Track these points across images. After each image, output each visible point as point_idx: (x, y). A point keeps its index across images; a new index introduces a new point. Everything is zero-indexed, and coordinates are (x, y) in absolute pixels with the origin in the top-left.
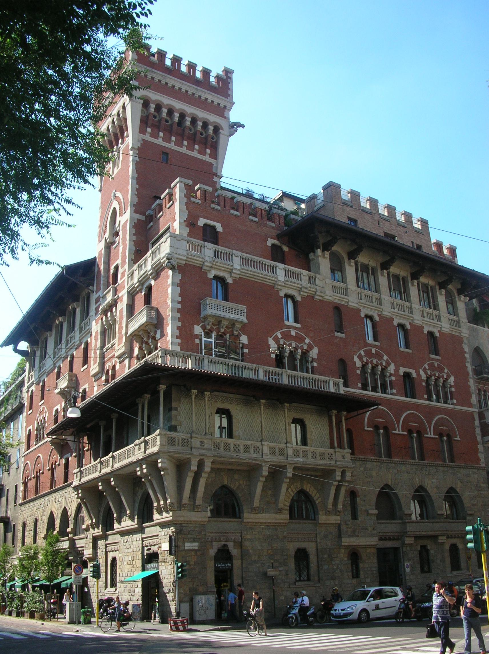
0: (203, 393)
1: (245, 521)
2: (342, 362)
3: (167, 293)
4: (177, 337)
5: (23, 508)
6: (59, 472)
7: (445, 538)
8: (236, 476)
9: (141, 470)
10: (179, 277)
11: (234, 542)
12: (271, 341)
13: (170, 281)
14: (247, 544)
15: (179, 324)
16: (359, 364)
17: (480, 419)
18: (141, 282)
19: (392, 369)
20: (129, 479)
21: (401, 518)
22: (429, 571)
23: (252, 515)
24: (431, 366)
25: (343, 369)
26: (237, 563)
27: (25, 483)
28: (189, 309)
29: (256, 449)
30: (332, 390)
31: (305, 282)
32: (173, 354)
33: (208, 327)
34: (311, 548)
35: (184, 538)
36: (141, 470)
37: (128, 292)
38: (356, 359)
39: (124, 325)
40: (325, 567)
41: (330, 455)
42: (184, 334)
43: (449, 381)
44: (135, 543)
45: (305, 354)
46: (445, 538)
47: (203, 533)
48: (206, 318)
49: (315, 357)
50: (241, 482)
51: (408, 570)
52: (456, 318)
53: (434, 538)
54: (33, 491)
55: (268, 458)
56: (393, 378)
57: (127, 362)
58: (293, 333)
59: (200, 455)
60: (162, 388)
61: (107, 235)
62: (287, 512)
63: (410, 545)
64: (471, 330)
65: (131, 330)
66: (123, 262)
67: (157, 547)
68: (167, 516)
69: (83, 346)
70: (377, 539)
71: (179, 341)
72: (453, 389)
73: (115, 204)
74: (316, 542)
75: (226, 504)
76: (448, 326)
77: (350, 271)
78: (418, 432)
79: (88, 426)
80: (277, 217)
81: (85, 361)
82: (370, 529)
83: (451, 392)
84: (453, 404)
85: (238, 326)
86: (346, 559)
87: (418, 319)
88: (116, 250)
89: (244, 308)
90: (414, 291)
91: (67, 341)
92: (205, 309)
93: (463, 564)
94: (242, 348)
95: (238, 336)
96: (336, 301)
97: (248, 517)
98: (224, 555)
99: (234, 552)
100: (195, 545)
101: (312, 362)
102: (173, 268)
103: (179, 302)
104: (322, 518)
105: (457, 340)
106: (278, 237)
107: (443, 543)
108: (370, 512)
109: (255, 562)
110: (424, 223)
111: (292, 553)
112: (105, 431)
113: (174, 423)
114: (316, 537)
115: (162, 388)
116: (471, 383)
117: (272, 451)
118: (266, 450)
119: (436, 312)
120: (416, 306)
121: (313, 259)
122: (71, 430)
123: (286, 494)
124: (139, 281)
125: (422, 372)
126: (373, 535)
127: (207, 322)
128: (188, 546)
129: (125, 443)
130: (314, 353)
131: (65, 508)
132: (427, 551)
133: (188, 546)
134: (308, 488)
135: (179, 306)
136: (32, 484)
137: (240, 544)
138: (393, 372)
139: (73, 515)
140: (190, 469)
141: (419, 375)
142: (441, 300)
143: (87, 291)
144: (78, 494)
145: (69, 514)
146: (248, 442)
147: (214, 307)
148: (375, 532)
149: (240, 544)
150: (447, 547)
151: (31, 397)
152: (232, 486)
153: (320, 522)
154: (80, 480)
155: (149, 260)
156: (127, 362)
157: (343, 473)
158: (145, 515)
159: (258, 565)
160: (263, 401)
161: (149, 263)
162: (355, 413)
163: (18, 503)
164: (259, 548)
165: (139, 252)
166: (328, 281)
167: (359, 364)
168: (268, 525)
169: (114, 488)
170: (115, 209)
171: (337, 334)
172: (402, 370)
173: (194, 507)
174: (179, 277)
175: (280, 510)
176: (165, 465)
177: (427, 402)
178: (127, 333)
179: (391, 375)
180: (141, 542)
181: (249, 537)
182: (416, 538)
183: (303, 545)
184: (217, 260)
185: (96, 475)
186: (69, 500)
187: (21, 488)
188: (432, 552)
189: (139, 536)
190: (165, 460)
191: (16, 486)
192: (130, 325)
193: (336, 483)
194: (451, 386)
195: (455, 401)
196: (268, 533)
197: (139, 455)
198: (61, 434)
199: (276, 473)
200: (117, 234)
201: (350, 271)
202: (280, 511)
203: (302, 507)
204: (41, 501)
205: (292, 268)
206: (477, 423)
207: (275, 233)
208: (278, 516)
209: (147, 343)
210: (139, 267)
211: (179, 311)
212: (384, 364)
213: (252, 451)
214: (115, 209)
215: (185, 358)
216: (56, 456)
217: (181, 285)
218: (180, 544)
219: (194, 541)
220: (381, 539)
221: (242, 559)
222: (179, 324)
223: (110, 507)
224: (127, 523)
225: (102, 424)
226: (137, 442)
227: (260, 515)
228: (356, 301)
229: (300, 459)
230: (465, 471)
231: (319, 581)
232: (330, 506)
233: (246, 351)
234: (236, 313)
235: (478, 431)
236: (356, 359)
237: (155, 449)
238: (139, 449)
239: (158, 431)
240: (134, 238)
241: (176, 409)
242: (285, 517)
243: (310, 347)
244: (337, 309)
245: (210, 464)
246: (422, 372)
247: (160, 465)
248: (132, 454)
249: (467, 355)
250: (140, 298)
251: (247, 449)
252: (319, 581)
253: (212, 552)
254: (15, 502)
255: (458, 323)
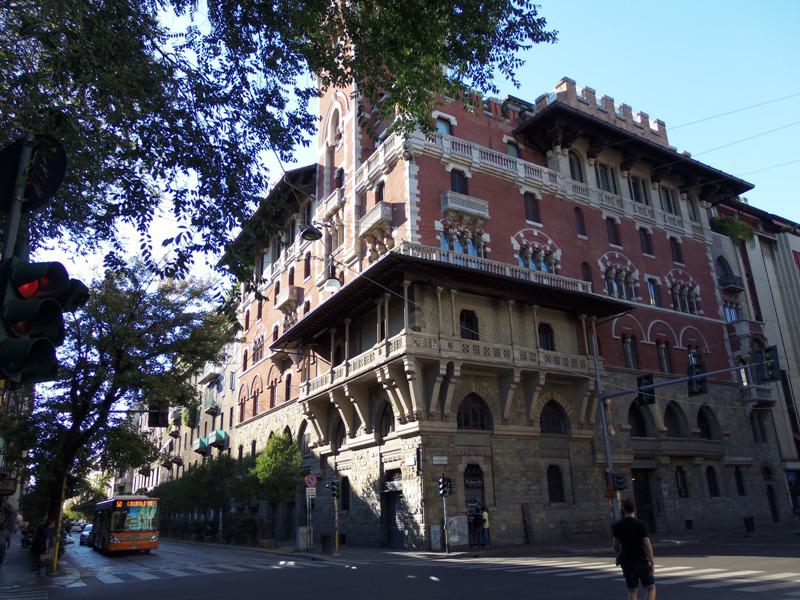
0: (449, 291)
1: (495, 433)
2: (585, 265)
3: (402, 186)
4: (418, 232)
5: (239, 430)
6: (281, 389)
7: (701, 459)
8: (485, 384)
9: (383, 375)
10: (416, 168)
11: (485, 456)
12: (513, 241)
13: (407, 173)
14: (497, 458)
15: (419, 219)
16: (603, 268)
17: (729, 332)
18: (372, 180)
19: (636, 274)
20: (369, 390)
21: (655, 435)
22: (687, 496)
23: (503, 427)
24: (676, 274)
25: (587, 271)
26: (488, 480)
27: (242, 405)
28: (429, 201)
29: (507, 354)
30: (580, 289)
31: (546, 180)
32: (415, 247)
33: (449, 223)
34: (564, 465)
35: (432, 452)
36: (383, 375)
37: (357, 193)
38: (600, 263)
39: (353, 225)
40: (580, 487)
41: (583, 362)
42: (424, 229)
43: (695, 290)
44: (371, 459)
45: (548, 255)
46: (701, 459)
47: (452, 445)
48: (446, 212)
49: (559, 259)
50: (490, 390)
51: (665, 493)
52: (698, 225)
53: (688, 458)
54: (251, 413)
55: (520, 363)
56: (638, 285)
57: (357, 265)
58: (536, 234)
59: (449, 358)
60: (407, 283)
61: (329, 139)
62: (538, 424)
63: (666, 465)
64: (715, 238)
65: (363, 231)
66: (349, 163)
67: (399, 462)
68: (413, 426)
69: (304, 257)
70: (632, 457)
71: (420, 236)
72: (699, 299)
73: (337, 105)
74: (569, 458)
75: (475, 415)
76: (691, 232)
77: (590, 172)
78: (667, 343)
79: (316, 336)
80: (511, 113)
81: (307, 272)
82: (624, 446)
83: (697, 302)
84: (700, 315)
85: (480, 222)
86: (600, 478)
87: (660, 223)
88: (340, 153)
89: (485, 203)
90: (655, 195)
91: (286, 255)
92: (446, 202)
93: (722, 490)
94: (484, 247)
95: (480, 234)
96: (577, 202)
97: (499, 428)
98: (473, 471)
99: (485, 468)
100: (444, 460)
101: (555, 264)
102: (409, 158)
103: (418, 196)
104: (575, 432)
105: (702, 248)
106: (514, 134)
107: (699, 465)
108: (624, 427)
109: (508, 479)
110: (661, 124)
111: (545, 470)
112: (336, 339)
113: (417, 324)
114: (569, 452)
115: (407, 283)
116: (717, 293)
117: (523, 357)
118: (517, 355)
119: (678, 218)
120: (658, 210)
121: (551, 158)
122: (294, 343)
123: (537, 404)
124: (369, 179)
125: (667, 280)
126: (626, 453)
127: (448, 218)
128: (437, 460)
129: (358, 351)
130: (558, 254)
131: (287, 426)
132: (683, 473)
133: (437, 460)
134: (559, 398)
135: (418, 200)
136: (249, 405)
137: (490, 459)
138: (637, 278)
139: (297, 434)
140: (438, 374)
141: (664, 282)
142: (684, 206)
143: (306, 202)
144: (305, 409)
145: (292, 432)
146: (499, 346)
147: (455, 201)
148: (630, 449)
149: (490, 459)
150: (704, 470)
151: (248, 316)
152: (481, 394)
153: (573, 436)
154: (308, 394)
155: (381, 154)
156: (357, 266)
157: (450, 367)
158: (381, 423)
159: (510, 482)
160: (512, 302)
161: (381, 156)
162: (606, 319)
163: (234, 425)
164: (511, 463)
165: (366, 152)
166: (569, 179)
167: (603, 268)
168: (519, 438)
169: (348, 398)
170: (336, 110)
171: (580, 236)
172: (647, 277)
173: (444, 417)
174: (417, 168)
175: (531, 421)
176: (413, 369)
177: (673, 311)
178: (357, 235)
179: (636, 281)
180: (378, 457)
181: (500, 451)
182: (673, 457)
183: (555, 462)
184: (455, 151)
185: (328, 386)
186: (292, 417)
187: (237, 410)
188: (689, 474)
189: (375, 450)
190: (412, 363)
191: (232, 409)
192: (362, 225)
193: (589, 394)
194: (697, 296)
195: (702, 312)
196: (519, 447)
197: (380, 358)
198: (285, 347)
199: (529, 377)
200: (339, 136)
201: (590, 172)
202: (531, 423)
203: (554, 419)
204: (260, 420)
205: (531, 164)
206: (726, 336)
207: (510, 129)
208: (531, 428)
209: (381, 244)
210: (369, 163)
211: (418, 205)
212: (628, 269)
213: (502, 355)
214: (336, 110)
215: (431, 252)
216: (276, 372)
217: (419, 177)
218: (428, 458)
219: (443, 455)
220: (635, 458)
221: (493, 476)
222: (419, 219)
223: (340, 416)
224: (363, 437)
225: (333, 331)
226: (377, 345)
227: (512, 427)
228: (598, 202)
229: (552, 366)
230: (717, 387)
231: (574, 502)
232: (582, 419)
233: (488, 250)
234: (479, 207)
235: (728, 345)
236: (600, 263)
237: (401, 351)
238: (380, 353)
239: (403, 331)
240: (360, 137)
241: (419, 309)
242: (536, 429)
243: (553, 249)
244: (578, 209)
245: (459, 368)
246: (667, 280)
247: (406, 368)
248: (372, 359)
249: (711, 264)
250: (371, 195)
251: (497, 353)
252: (574, 502)
253: (462, 468)
254: (231, 425)
255: (700, 229)
